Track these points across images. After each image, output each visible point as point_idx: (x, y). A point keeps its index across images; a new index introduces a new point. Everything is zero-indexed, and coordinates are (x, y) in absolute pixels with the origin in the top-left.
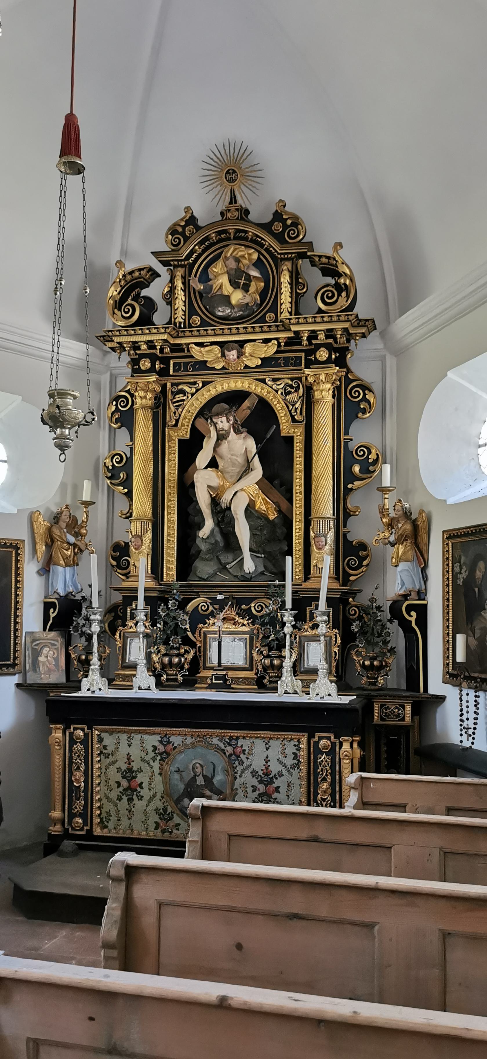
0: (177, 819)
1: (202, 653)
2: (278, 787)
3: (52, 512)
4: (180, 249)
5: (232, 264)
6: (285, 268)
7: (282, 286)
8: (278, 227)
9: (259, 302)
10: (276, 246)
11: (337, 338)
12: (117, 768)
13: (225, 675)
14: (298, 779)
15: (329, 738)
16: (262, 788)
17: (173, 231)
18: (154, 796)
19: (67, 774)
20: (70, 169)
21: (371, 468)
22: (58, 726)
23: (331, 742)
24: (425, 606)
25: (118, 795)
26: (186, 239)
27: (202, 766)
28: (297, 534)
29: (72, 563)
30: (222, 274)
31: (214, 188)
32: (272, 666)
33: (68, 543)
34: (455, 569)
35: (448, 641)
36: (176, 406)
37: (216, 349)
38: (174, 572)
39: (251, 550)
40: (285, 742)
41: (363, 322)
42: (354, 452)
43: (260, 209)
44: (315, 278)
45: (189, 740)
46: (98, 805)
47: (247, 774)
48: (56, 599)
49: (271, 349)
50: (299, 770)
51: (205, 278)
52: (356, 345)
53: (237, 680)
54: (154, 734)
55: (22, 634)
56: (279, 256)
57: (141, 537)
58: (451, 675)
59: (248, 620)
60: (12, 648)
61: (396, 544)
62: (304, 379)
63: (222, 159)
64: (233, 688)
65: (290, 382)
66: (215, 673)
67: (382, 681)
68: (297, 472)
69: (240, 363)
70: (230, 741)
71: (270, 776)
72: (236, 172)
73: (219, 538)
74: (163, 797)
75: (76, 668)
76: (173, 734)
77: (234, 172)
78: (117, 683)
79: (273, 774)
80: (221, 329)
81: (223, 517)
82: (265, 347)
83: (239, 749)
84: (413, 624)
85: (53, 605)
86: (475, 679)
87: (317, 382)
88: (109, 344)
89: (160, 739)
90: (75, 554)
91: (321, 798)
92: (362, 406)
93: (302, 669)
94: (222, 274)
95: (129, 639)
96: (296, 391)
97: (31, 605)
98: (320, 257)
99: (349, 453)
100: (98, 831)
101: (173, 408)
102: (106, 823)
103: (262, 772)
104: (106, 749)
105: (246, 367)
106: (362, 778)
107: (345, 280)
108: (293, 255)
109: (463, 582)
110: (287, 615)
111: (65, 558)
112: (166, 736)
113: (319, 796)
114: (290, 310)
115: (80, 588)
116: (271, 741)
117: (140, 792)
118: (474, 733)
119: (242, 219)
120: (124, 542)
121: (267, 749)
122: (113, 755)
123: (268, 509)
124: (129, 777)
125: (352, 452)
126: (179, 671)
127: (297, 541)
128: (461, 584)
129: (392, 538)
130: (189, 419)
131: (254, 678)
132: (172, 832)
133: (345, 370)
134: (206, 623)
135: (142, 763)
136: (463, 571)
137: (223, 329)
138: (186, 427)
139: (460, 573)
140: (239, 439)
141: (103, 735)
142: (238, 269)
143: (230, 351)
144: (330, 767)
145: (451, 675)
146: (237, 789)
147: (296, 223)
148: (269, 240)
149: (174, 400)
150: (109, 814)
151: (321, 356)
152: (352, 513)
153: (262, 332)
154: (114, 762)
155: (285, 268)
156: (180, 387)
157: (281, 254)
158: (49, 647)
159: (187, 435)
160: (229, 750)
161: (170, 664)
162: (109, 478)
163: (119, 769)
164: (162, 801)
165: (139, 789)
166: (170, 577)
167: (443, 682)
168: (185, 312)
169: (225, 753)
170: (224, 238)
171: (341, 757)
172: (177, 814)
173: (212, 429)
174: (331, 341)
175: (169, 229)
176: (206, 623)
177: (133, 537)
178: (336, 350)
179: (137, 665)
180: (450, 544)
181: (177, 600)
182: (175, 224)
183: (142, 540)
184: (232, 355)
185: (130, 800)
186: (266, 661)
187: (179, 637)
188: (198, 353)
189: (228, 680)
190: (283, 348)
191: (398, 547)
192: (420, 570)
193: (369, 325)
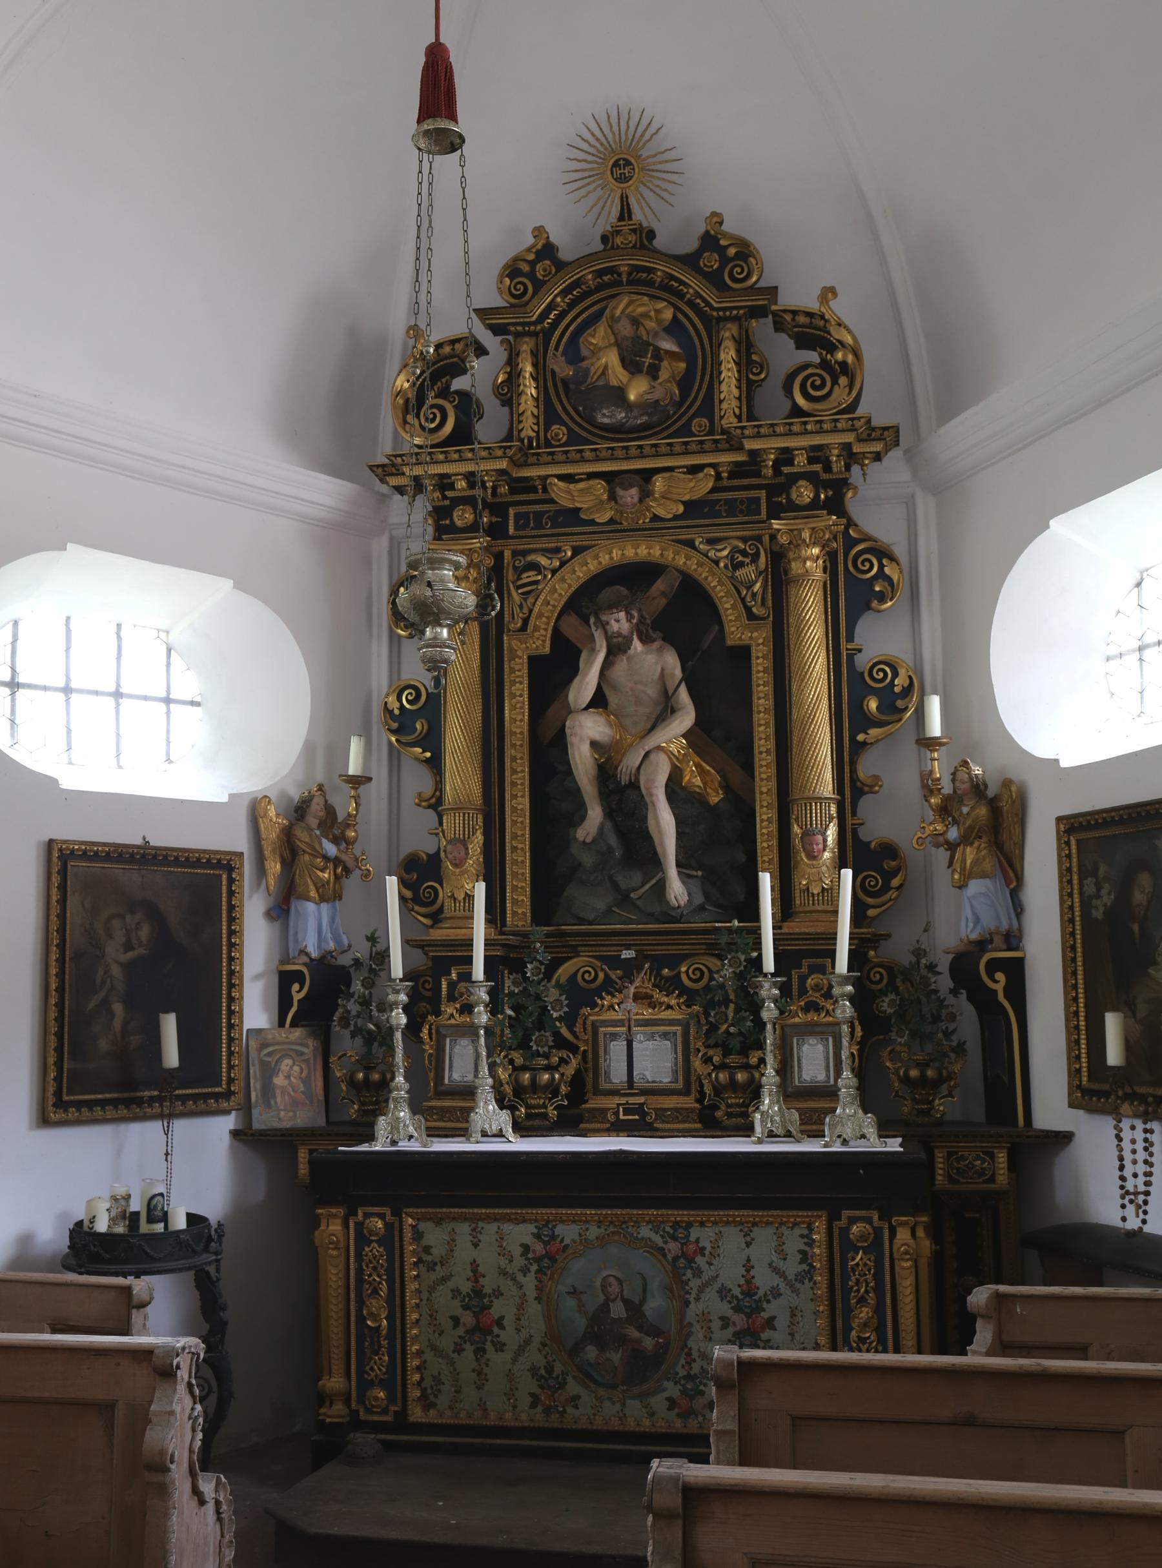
0: (573, 1387)
1: (590, 1064)
2: (773, 1318)
3: (291, 799)
4: (527, 303)
5: (625, 329)
6: (727, 334)
7: (723, 368)
8: (711, 261)
9: (677, 399)
10: (710, 295)
11: (830, 462)
12: (452, 1291)
13: (643, 1104)
14: (811, 1302)
15: (869, 1220)
16: (740, 1321)
17: (512, 271)
18: (528, 1342)
19: (353, 1304)
20: (437, 142)
21: (900, 704)
22: (334, 1211)
23: (874, 1229)
25: (455, 1343)
26: (539, 285)
27: (617, 1279)
28: (765, 831)
29: (331, 895)
30: (606, 347)
31: (589, 193)
32: (733, 1084)
33: (326, 858)
34: (1086, 888)
35: (1077, 1027)
36: (522, 594)
37: (600, 486)
38: (526, 909)
39: (678, 865)
40: (783, 1229)
41: (879, 432)
42: (866, 675)
43: (675, 230)
44: (783, 354)
45: (594, 1232)
46: (416, 1362)
47: (711, 1294)
48: (305, 964)
49: (703, 486)
50: (811, 1284)
51: (573, 354)
52: (864, 475)
53: (661, 1113)
54: (524, 1221)
55: (242, 1034)
56: (715, 314)
57: (464, 843)
58: (1086, 1092)
59: (679, 996)
61: (958, 845)
62: (766, 539)
64: (657, 1130)
66: (623, 1100)
67: (941, 1108)
68: (759, 712)
69: (652, 513)
70: (675, 1230)
71: (756, 1297)
73: (613, 840)
74: (544, 1345)
75: (344, 1098)
76: (562, 1222)
77: (628, 163)
79: (761, 1293)
80: (609, 448)
82: (691, 480)
83: (692, 1247)
84: (1001, 997)
85: (298, 977)
86: (1143, 1099)
87: (797, 543)
88: (394, 481)
89: (535, 1231)
90: (337, 878)
91: (858, 1337)
92: (877, 589)
93: (790, 1089)
94: (606, 347)
95: (448, 1040)
96: (753, 561)
97: (257, 977)
98: (795, 313)
99: (856, 677)
100: (417, 1414)
101: (517, 598)
102: (432, 1398)
104: (430, 1254)
105: (655, 518)
106: (998, 1296)
107: (845, 355)
108: (742, 312)
109: (1104, 913)
110: (766, 985)
111: (320, 885)
112: (546, 1225)
113: (854, 1333)
114: (737, 411)
115: (346, 943)
116: (755, 1229)
117: (498, 1336)
118: (1146, 1202)
119: (643, 247)
120: (427, 854)
121: (748, 1244)
122: (442, 1265)
123: (705, 783)
125: (863, 673)
126: (550, 1099)
127: (765, 845)
128: (1100, 917)
129: (953, 834)
130: (548, 618)
131: (693, 1110)
132: (564, 1411)
133: (844, 521)
136: (1104, 892)
137: (612, 449)
138: (543, 632)
139: (1098, 896)
141: (423, 1226)
142: (637, 339)
143: (626, 489)
144: (874, 1275)
145: (1086, 1092)
146: (690, 1324)
147: (746, 251)
148: (694, 285)
149: (520, 583)
150: (437, 1380)
151: (801, 495)
152: (866, 789)
153: (687, 453)
154: (445, 1279)
155: (727, 334)
156: (530, 558)
157: (718, 309)
158: (292, 1058)
159: (544, 647)
160: (673, 1247)
161: (534, 1086)
162: (393, 732)
163: (456, 1292)
164: (544, 1353)
165: (496, 1330)
166: (520, 920)
167: (1071, 1105)
168: (537, 417)
169: (664, 1256)
170: (610, 282)
171: (896, 1256)
172: (575, 1377)
173: (598, 635)
174: (817, 467)
175: (506, 266)
176: (596, 1005)
177: (449, 842)
178: (826, 484)
179: (476, 1088)
180: (1073, 842)
181: (541, 963)
182: (517, 259)
183: (467, 849)
184: (631, 495)
185: (480, 1351)
186: (721, 1076)
187: (548, 1034)
189: (647, 1114)
190: (725, 483)
191: (964, 851)
192: (1007, 892)
193: (889, 436)
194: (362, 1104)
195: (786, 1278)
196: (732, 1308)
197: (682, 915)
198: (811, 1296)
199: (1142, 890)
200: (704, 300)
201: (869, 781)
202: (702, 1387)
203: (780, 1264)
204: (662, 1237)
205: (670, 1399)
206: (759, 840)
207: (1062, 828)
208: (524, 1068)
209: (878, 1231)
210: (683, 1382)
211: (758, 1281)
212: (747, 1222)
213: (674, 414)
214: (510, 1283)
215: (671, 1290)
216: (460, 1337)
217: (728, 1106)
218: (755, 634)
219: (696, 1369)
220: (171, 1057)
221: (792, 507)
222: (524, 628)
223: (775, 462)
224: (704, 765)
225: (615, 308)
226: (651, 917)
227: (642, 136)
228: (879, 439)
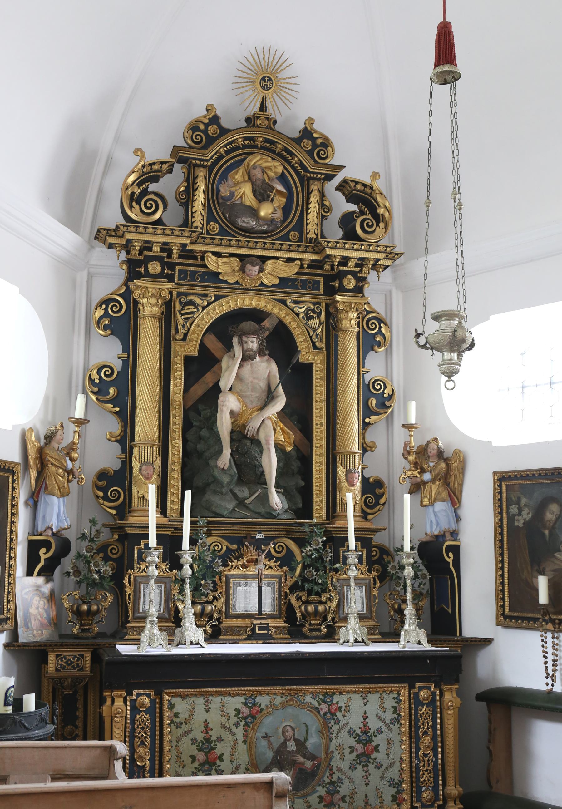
2: (378, 746)
12: (192, 740)
15: (429, 688)
17: (194, 127)
23: (432, 692)
24: (458, 547)
27: (293, 729)
28: (317, 468)
34: (511, 510)
37: (235, 262)
41: (393, 255)
45: (278, 700)
49: (289, 271)
50: (399, 725)
52: (378, 277)
54: (238, 695)
58: (511, 618)
59: (275, 562)
60: (6, 598)
63: (258, 62)
64: (274, 639)
70: (325, 697)
71: (369, 734)
72: (272, 81)
75: (70, 622)
76: (261, 695)
77: (270, 80)
78: (131, 637)
79: (372, 731)
82: (286, 266)
89: (244, 701)
91: (423, 754)
92: (378, 339)
95: (142, 585)
101: (181, 320)
103: (360, 730)
105: (262, 284)
108: (323, 176)
109: (524, 523)
113: (420, 752)
116: (369, 695)
117: (219, 766)
121: (365, 704)
122: (186, 724)
124: (206, 748)
126: (208, 622)
128: (521, 525)
130: (198, 334)
131: (284, 628)
134: (228, 565)
135: (223, 730)
138: (195, 343)
140: (262, 362)
141: (174, 700)
145: (506, 617)
146: (332, 752)
147: (326, 144)
149: (182, 312)
152: (368, 449)
155: (316, 188)
156: (191, 298)
160: (324, 707)
162: (94, 393)
163: (194, 741)
165: (218, 762)
166: (174, 513)
167: (497, 625)
168: (203, 216)
169: (319, 712)
170: (251, 145)
174: (165, 255)
182: (198, 121)
188: (212, 263)
189: (270, 630)
190: (306, 270)
191: (431, 487)
194: (81, 625)
195: (385, 722)
196: (356, 741)
197: (278, 514)
198: (399, 732)
199: (552, 512)
201: (370, 445)
202: (338, 788)
203: (381, 714)
204: (318, 701)
205: (320, 797)
207: (496, 477)
208: (307, 603)
209: (434, 694)
210: (327, 786)
211: (370, 725)
212: (365, 691)
213: (281, 226)
214: (228, 733)
215: (322, 732)
216: (196, 768)
217: (310, 625)
218: (316, 358)
219: (335, 778)
220: (543, 598)
222: (184, 339)
225: (251, 161)
227: (281, 66)
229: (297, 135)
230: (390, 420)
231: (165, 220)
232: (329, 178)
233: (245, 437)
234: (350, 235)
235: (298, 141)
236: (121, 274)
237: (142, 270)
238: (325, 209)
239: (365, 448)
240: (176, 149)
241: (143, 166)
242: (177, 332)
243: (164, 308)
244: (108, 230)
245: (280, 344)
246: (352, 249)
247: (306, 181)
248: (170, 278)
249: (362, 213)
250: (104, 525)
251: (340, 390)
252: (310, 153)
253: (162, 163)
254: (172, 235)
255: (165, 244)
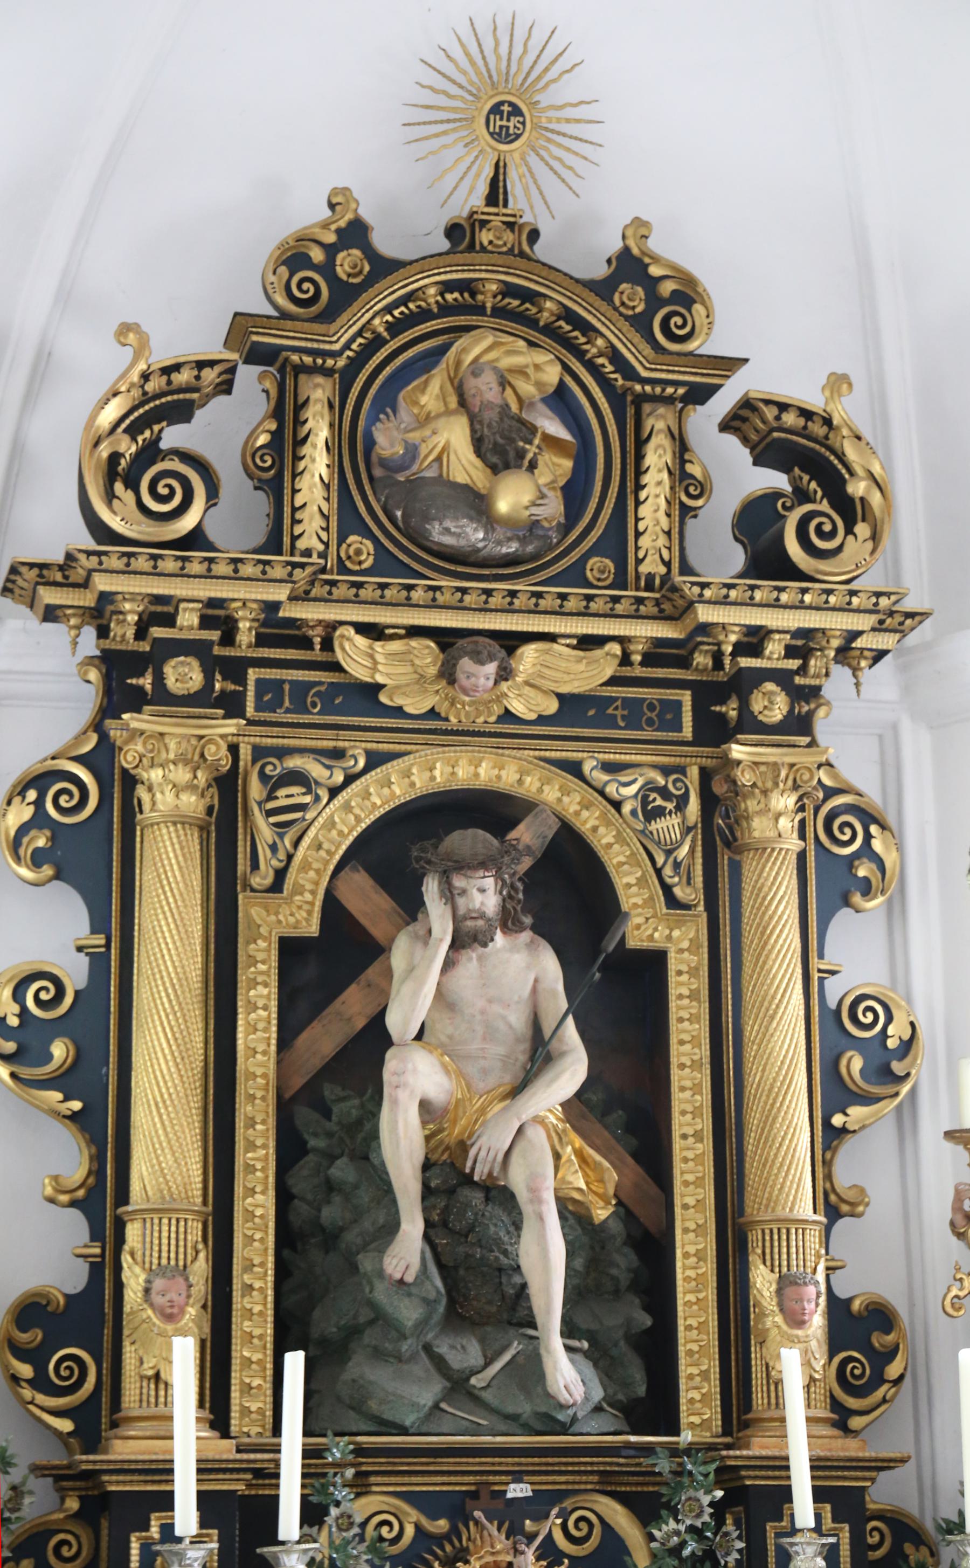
17: (293, 259)
28: (690, 1273)
36: (277, 825)
37: (426, 653)
41: (898, 618)
49: (589, 674)
52: (857, 685)
65: (661, 781)
77: (516, 111)
81: (446, 1211)
82: (579, 660)
92: (861, 873)
101: (265, 829)
105: (508, 716)
108: (681, 391)
125: (838, 1011)
130: (318, 871)
138: (308, 897)
140: (513, 949)
147: (688, 295)
149: (270, 805)
152: (845, 1208)
155: (660, 425)
156: (294, 763)
168: (326, 518)
174: (215, 635)
190: (639, 671)
197: (574, 1419)
200: (352, 340)
206: (680, 1290)
218: (676, 933)
221: (162, 696)
222: (277, 886)
223: (736, 645)
224: (591, 1152)
225: (465, 350)
226: (515, 1422)
227: (547, 70)
228: (895, 631)
229: (600, 271)
230: (907, 1118)
231: (212, 533)
232: (700, 395)
233: (468, 1180)
234: (768, 564)
235: (603, 289)
236: (86, 696)
237: (146, 682)
238: (689, 487)
239: (834, 1208)
240: (241, 324)
241: (145, 377)
242: (255, 866)
243: (213, 797)
244: (42, 566)
245: (566, 894)
246: (776, 604)
247: (630, 406)
248: (232, 706)
249: (802, 496)
250: (38, 1470)
251: (751, 1030)
252: (641, 323)
253: (201, 365)
254: (236, 577)
255: (213, 603)
